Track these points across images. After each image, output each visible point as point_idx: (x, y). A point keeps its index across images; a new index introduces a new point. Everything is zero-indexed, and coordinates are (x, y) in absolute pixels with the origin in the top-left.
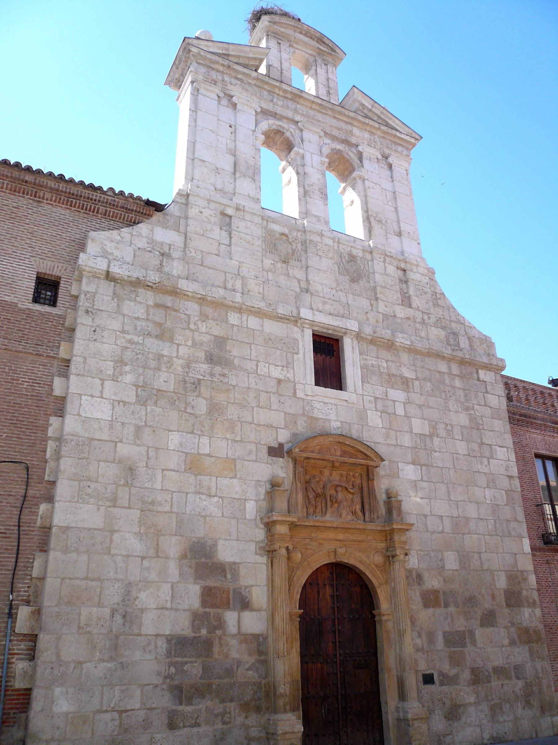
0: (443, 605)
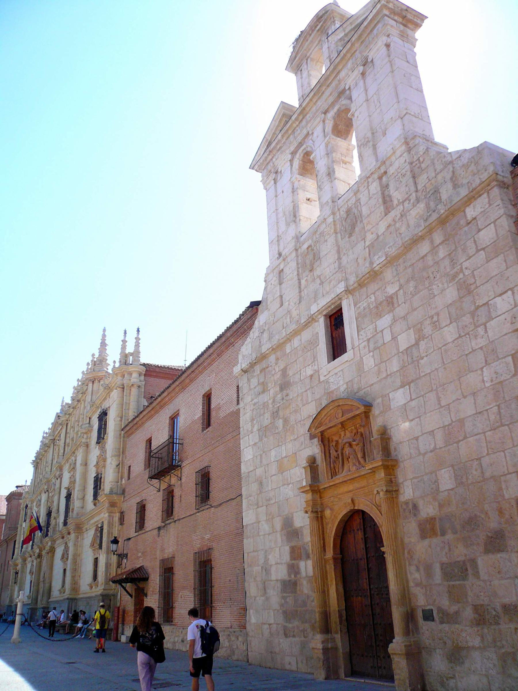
0: (439, 533)
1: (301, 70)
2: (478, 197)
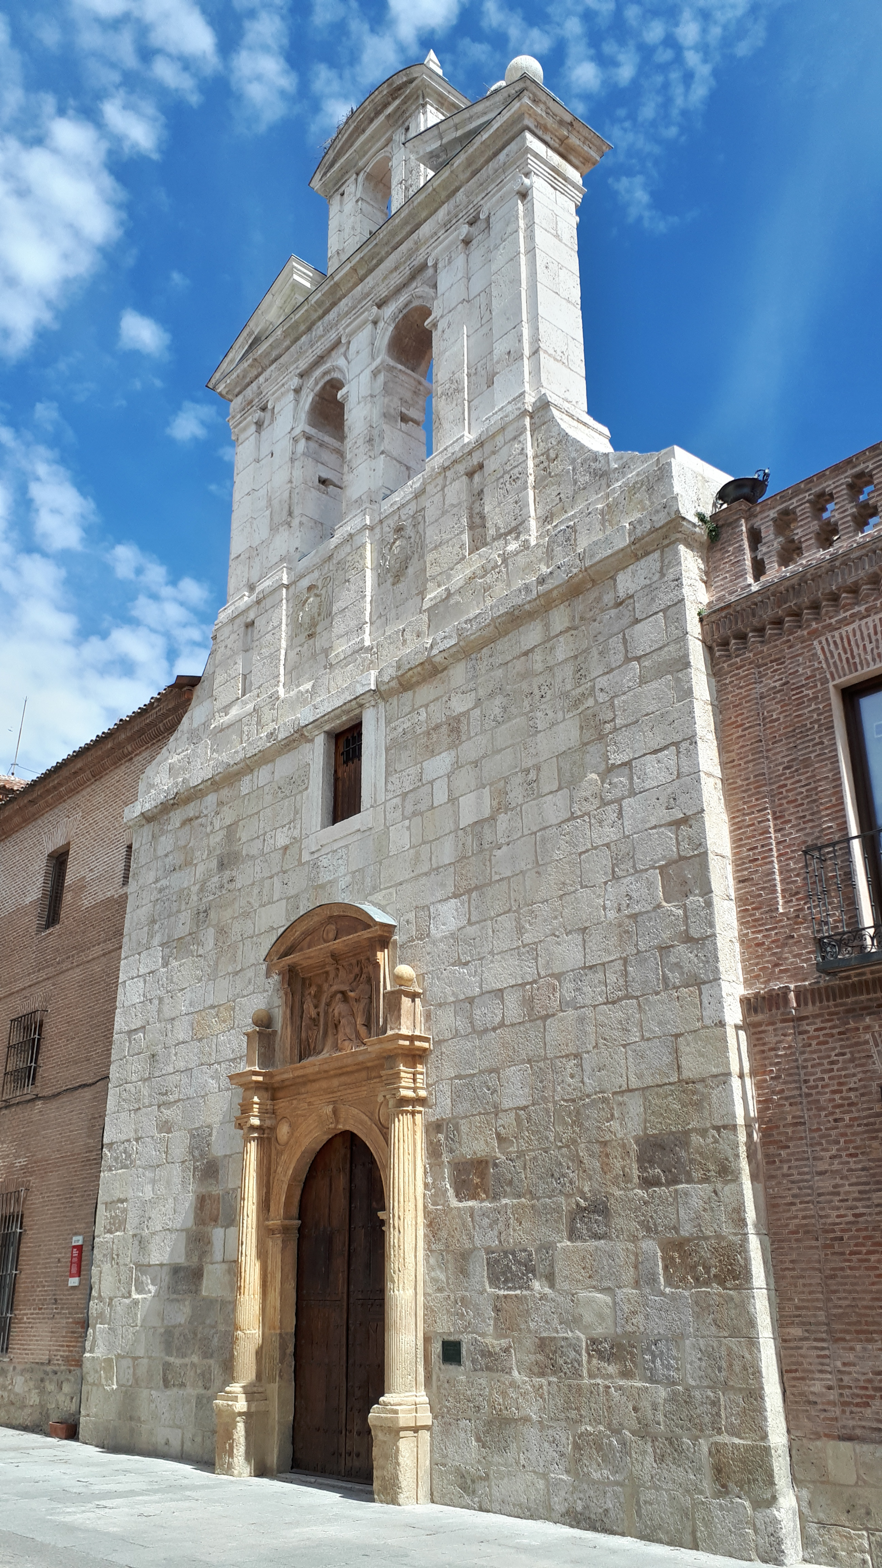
1: (342, 195)
2: (642, 557)
